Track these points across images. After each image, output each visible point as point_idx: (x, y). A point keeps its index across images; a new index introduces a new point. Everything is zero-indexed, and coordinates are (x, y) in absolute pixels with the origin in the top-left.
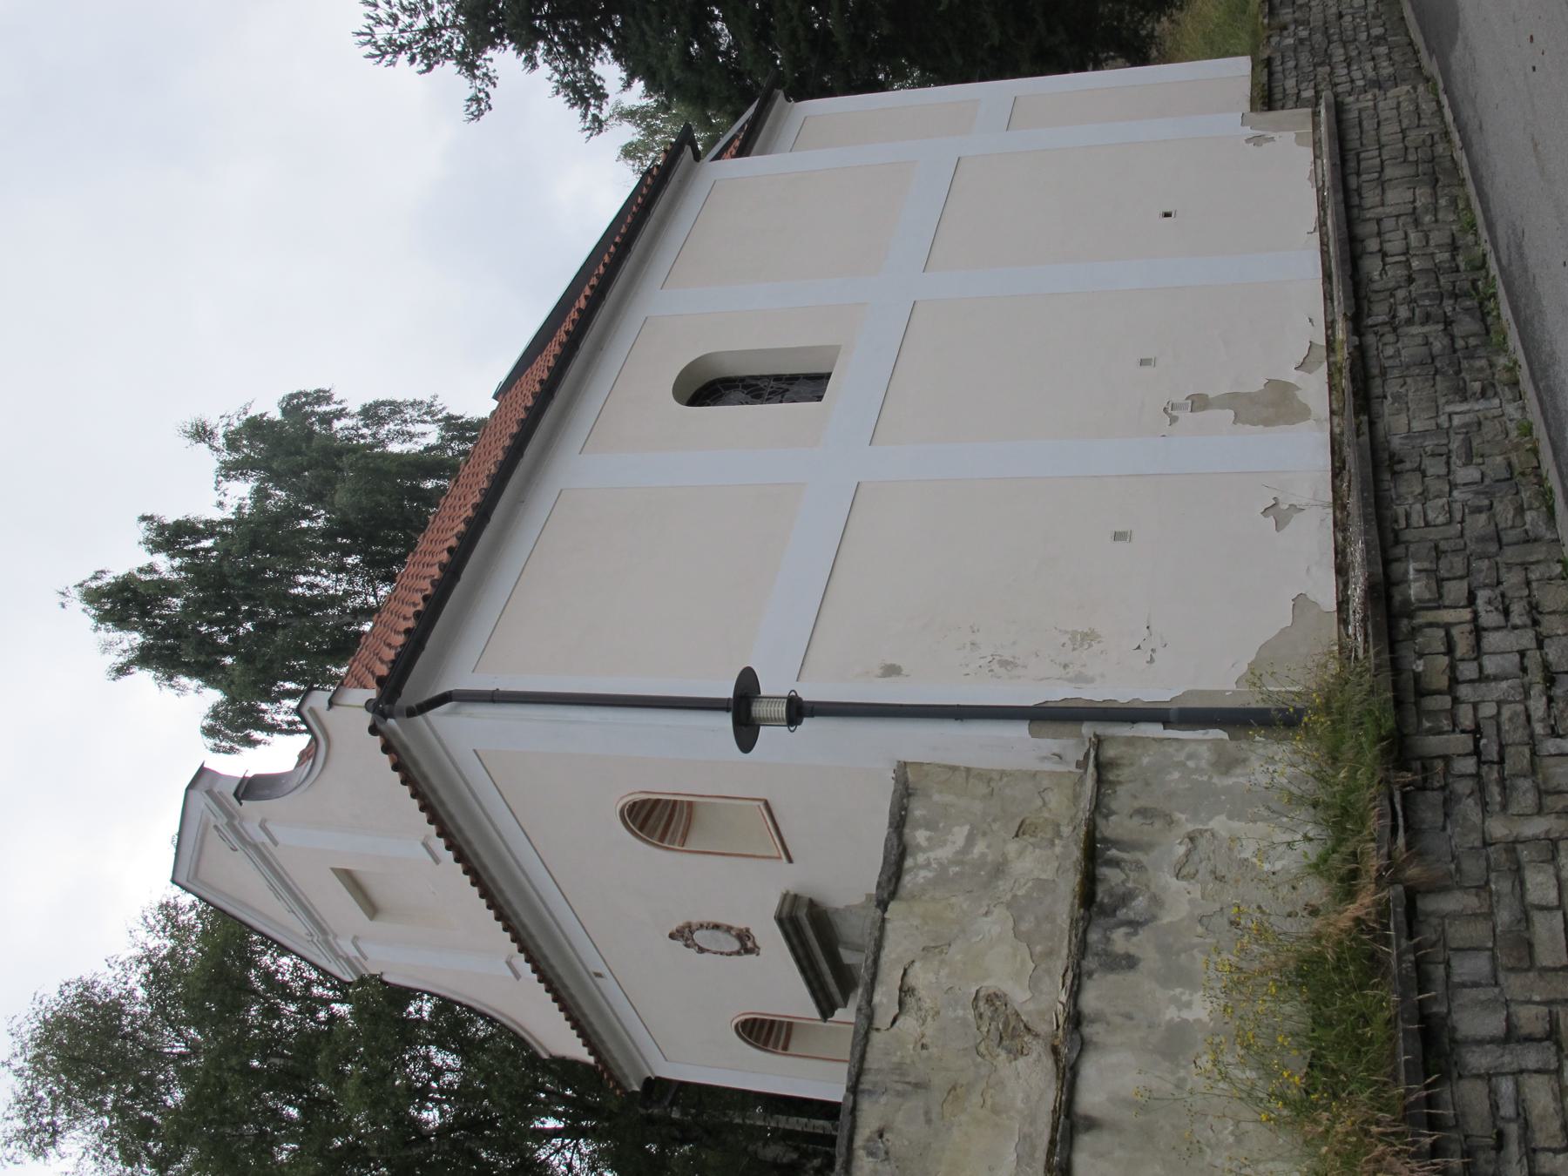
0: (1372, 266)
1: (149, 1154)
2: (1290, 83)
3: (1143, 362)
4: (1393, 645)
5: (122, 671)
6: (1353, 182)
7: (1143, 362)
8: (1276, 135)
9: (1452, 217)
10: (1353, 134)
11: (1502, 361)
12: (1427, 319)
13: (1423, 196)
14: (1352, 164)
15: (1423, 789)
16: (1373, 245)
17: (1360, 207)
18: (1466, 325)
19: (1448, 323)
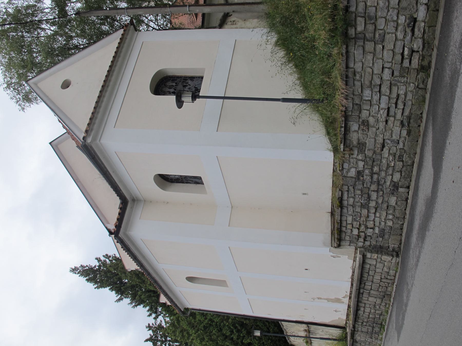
0: (361, 312)
1: (107, 22)
2: (350, 219)
3: (304, 194)
4: (355, 323)
5: (147, 340)
6: (362, 291)
7: (304, 194)
8: (341, 256)
9: (383, 308)
10: (365, 275)
11: (381, 336)
12: (370, 326)
13: (379, 301)
14: (363, 285)
15: (383, 60)
16: (362, 309)
17: (363, 288)
18: (377, 329)
19: (373, 327)
